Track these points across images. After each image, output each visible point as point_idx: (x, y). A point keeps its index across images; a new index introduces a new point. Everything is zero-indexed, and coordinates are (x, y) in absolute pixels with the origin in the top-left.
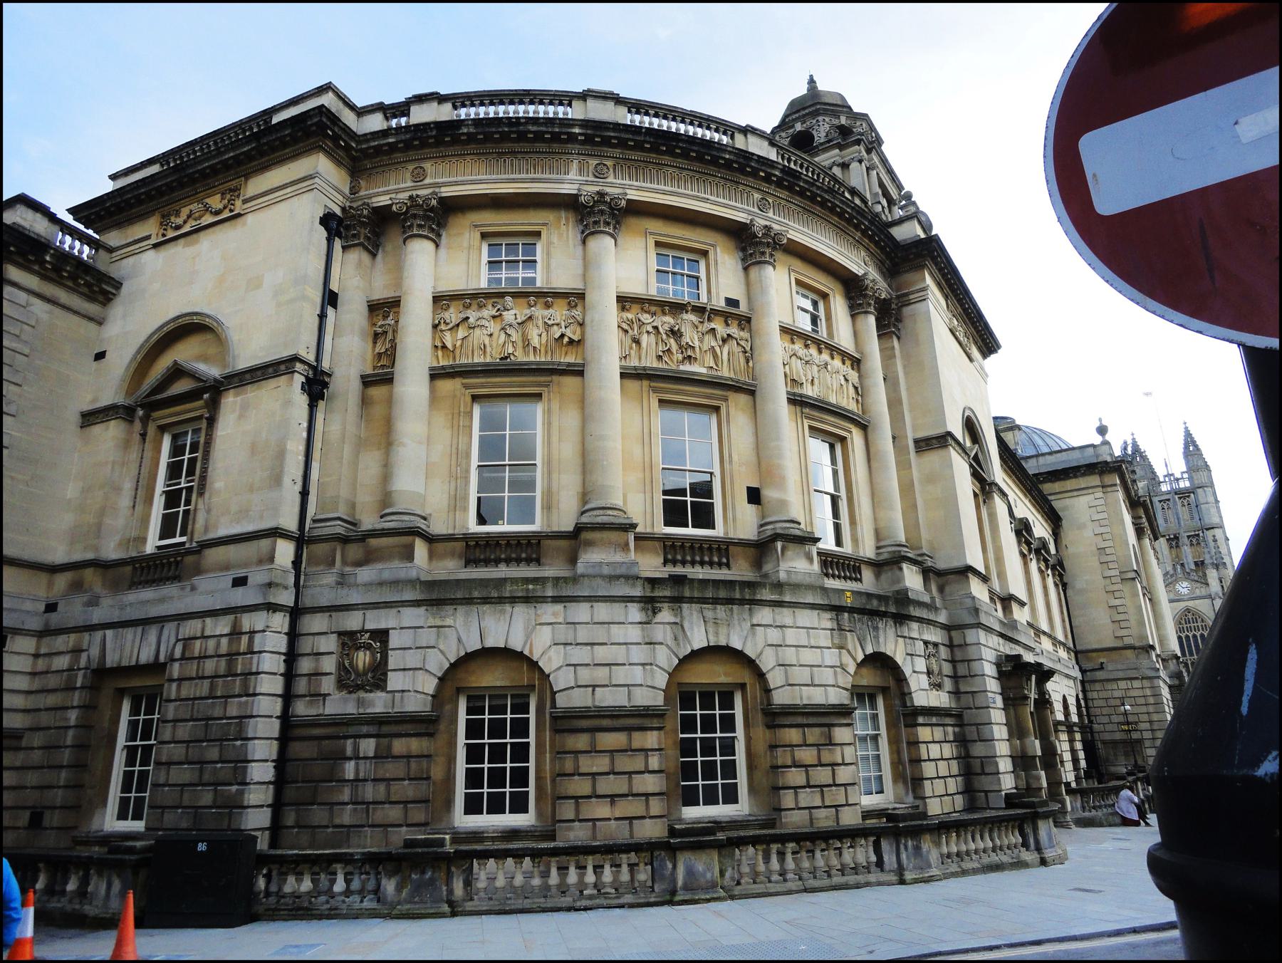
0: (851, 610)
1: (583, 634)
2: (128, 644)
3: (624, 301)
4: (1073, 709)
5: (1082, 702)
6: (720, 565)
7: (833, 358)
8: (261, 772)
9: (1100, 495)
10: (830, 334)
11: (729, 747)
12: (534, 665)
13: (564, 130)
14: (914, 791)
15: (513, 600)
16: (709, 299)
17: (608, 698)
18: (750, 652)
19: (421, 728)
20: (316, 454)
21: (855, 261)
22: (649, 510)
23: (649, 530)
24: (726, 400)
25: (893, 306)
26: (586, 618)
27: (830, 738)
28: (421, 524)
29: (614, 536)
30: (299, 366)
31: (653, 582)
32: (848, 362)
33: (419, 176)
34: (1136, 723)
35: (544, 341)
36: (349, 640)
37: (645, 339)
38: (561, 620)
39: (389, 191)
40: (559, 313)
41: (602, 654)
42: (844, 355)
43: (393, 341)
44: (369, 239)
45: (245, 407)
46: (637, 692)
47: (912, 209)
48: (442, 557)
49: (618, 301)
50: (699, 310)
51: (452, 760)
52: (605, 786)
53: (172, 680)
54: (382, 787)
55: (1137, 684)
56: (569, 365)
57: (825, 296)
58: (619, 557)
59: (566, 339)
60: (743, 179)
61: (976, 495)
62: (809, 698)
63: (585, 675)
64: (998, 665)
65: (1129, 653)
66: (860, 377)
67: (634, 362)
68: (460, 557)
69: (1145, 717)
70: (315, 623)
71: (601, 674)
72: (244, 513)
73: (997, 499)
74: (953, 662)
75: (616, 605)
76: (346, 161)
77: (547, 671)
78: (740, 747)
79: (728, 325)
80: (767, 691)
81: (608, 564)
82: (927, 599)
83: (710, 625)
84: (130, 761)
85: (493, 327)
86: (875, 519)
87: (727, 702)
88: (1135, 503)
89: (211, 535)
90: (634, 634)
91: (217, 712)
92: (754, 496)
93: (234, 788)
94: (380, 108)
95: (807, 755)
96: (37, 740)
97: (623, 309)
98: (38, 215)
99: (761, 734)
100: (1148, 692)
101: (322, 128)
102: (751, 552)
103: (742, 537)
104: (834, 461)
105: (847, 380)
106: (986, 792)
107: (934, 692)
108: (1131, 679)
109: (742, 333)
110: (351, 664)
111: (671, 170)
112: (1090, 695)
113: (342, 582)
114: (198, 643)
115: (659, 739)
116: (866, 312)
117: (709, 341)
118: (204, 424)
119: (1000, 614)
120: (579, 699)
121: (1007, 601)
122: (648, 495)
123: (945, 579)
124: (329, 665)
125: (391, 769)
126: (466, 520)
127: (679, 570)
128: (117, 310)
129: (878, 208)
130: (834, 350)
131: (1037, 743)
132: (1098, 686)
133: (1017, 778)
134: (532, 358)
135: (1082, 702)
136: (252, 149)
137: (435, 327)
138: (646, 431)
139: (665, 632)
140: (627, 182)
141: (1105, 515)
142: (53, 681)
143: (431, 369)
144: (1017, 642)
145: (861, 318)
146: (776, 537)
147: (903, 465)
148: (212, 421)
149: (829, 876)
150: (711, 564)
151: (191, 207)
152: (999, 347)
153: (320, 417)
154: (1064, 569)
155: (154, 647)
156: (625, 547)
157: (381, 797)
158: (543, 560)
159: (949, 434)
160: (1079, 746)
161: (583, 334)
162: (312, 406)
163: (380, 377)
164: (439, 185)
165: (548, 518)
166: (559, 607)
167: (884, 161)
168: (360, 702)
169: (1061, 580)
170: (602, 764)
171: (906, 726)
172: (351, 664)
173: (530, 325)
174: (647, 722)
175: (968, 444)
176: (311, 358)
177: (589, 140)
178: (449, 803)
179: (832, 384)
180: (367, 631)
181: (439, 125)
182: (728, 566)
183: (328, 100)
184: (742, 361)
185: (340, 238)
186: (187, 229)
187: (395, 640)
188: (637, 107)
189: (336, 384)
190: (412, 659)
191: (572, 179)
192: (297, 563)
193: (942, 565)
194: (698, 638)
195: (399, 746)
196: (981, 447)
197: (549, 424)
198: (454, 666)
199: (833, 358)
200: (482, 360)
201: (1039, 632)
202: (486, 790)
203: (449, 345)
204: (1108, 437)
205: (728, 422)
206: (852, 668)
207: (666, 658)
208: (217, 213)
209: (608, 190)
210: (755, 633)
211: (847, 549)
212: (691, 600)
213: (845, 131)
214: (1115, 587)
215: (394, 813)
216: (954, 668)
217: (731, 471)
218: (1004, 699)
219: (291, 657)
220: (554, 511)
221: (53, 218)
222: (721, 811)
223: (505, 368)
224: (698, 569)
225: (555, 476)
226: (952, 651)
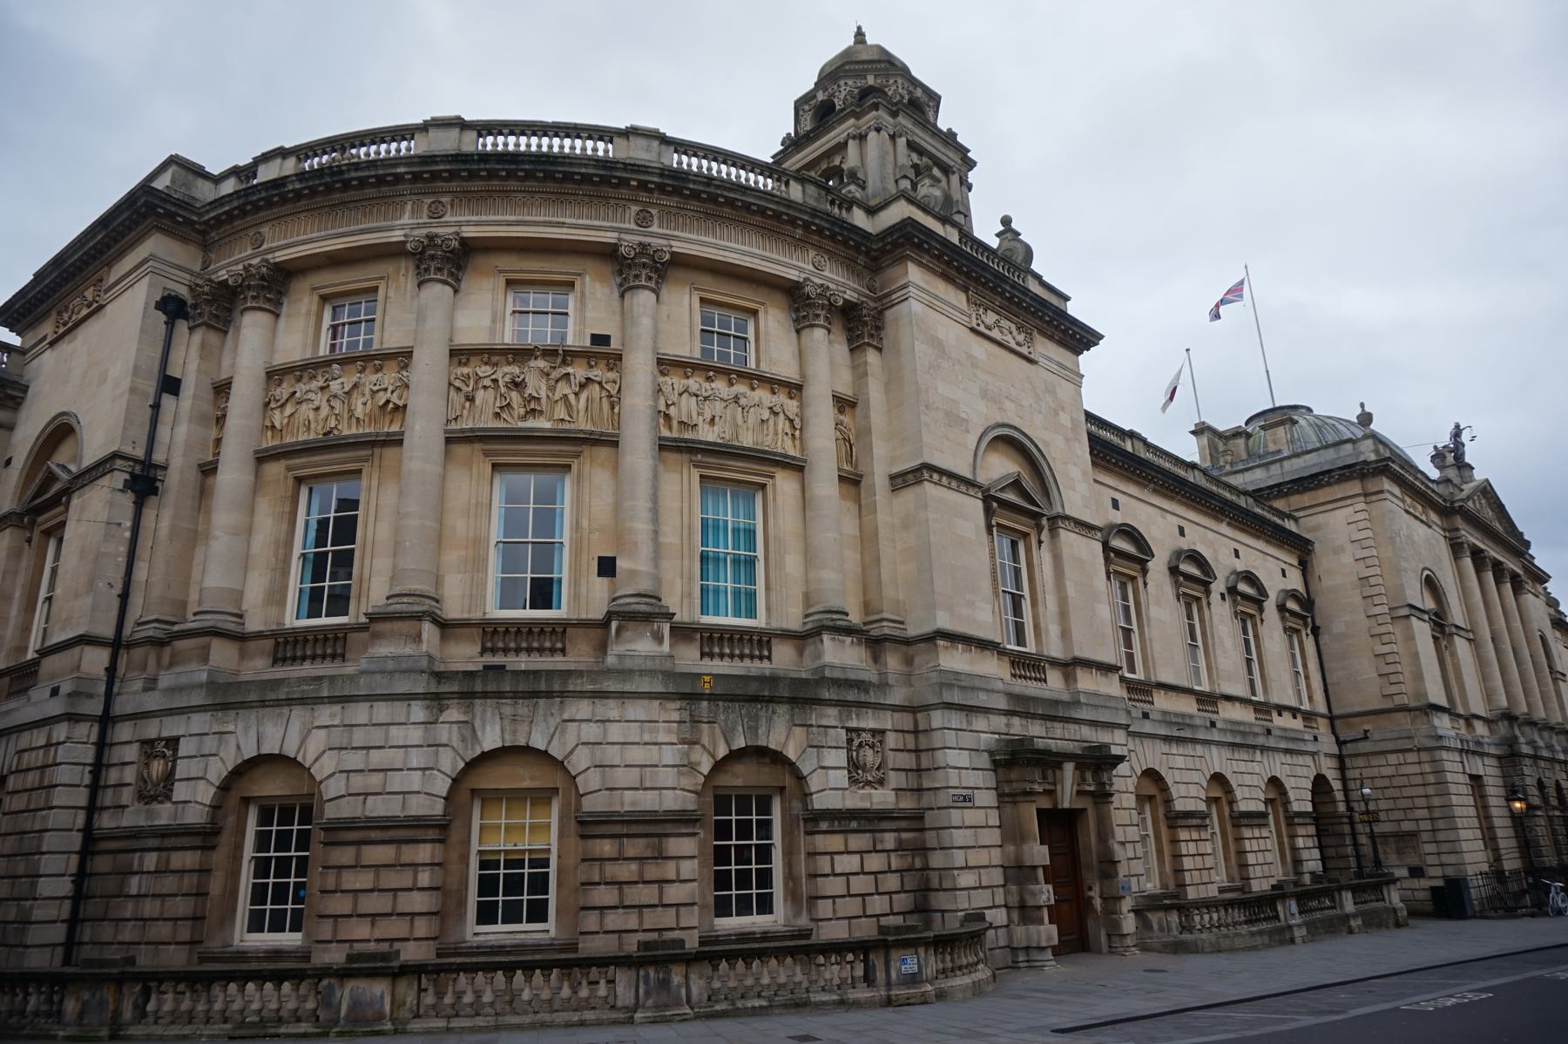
0: (712, 698)
1: (359, 737)
6: (553, 651)
9: (1362, 506)
11: (765, 854)
14: (809, 911)
15: (290, 702)
17: (378, 808)
26: (363, 719)
29: (405, 626)
30: (119, 463)
31: (470, 675)
36: (148, 747)
46: (413, 799)
51: (235, 874)
55: (1412, 757)
60: (611, 192)
62: (634, 803)
63: (358, 782)
65: (1401, 717)
66: (801, 406)
69: (1421, 802)
70: (124, 732)
71: (375, 781)
78: (777, 855)
83: (506, 721)
85: (319, 399)
86: (807, 581)
87: (765, 808)
90: (415, 735)
92: (607, 567)
95: (627, 871)
100: (1427, 768)
101: (151, 208)
106: (943, 911)
113: (151, 685)
117: (563, 389)
120: (348, 809)
123: (914, 647)
124: (130, 775)
127: (498, 659)
132: (1361, 762)
139: (450, 732)
141: (1369, 533)
143: (256, 452)
150: (541, 650)
162: (139, 506)
166: (337, 708)
170: (363, 880)
174: (419, 834)
176: (140, 453)
177: (417, 177)
178: (462, 916)
180: (162, 739)
182: (563, 651)
184: (606, 406)
187: (185, 748)
191: (404, 224)
194: (491, 739)
202: (500, 898)
203: (277, 425)
207: (450, 763)
212: (485, 695)
214: (1382, 629)
216: (918, 758)
222: (755, 922)
223: (330, 444)
224: (523, 657)
226: (917, 739)
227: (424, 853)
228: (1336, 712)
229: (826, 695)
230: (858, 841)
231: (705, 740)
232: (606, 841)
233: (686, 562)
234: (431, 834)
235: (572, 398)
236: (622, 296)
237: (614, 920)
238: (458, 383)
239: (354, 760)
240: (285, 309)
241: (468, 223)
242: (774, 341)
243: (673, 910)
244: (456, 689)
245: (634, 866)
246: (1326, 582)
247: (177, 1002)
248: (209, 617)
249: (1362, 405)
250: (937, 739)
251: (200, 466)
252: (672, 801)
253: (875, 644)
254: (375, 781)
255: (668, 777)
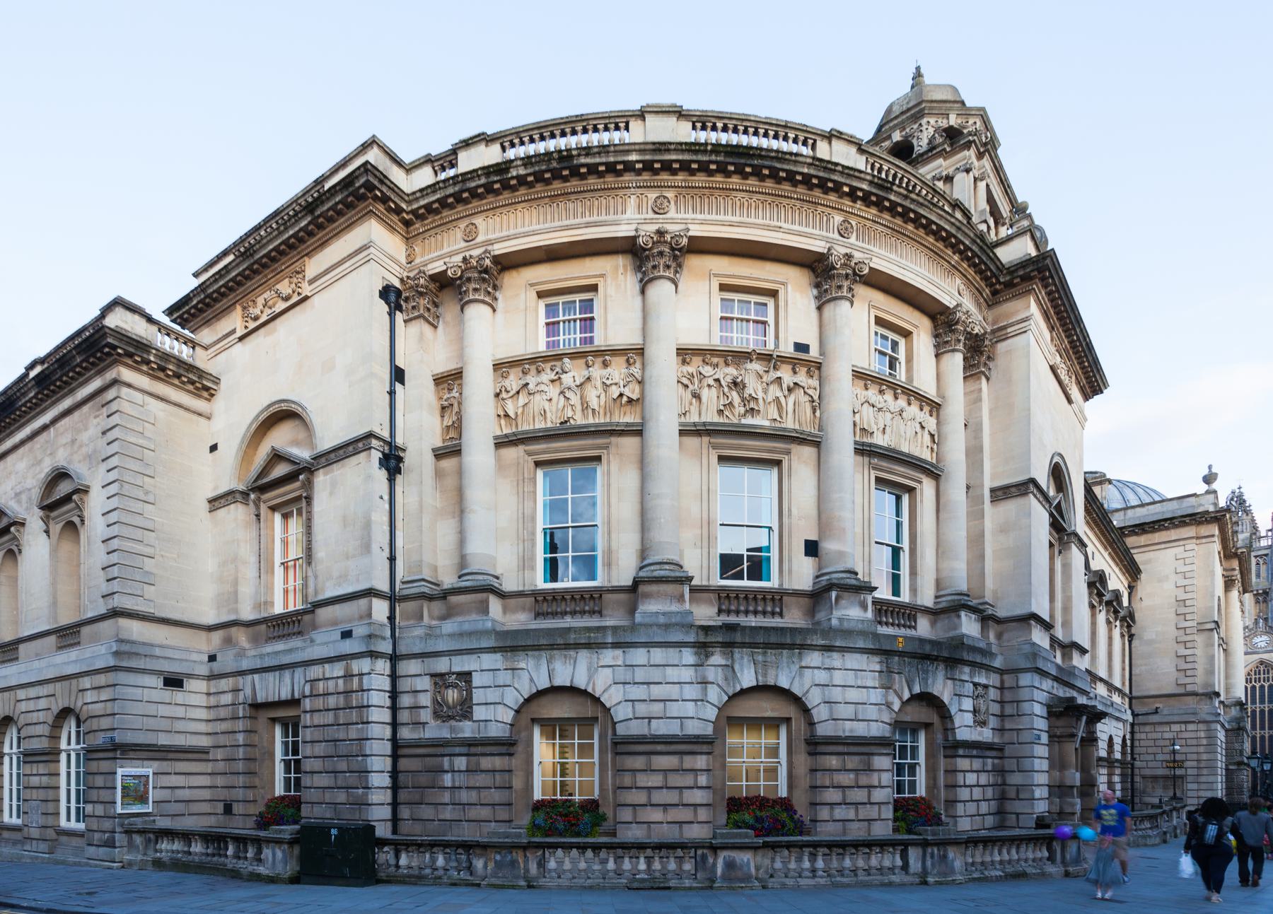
1: (640, 675)
2: (271, 686)
3: (685, 354)
4: (1117, 748)
5: (1129, 742)
6: (773, 614)
7: (909, 404)
8: (381, 780)
10: (910, 378)
11: (912, 768)
12: (596, 700)
13: (620, 159)
15: (577, 646)
16: (777, 346)
17: (660, 728)
18: (797, 690)
19: (503, 749)
20: (399, 524)
21: (948, 289)
22: (705, 565)
23: (705, 583)
24: (788, 453)
25: (987, 342)
27: (869, 764)
28: (495, 583)
30: (374, 443)
31: (706, 629)
32: (927, 409)
33: (469, 237)
34: (1183, 761)
35: (602, 403)
36: (440, 680)
37: (705, 393)
38: (620, 663)
39: (445, 251)
40: (617, 370)
41: (657, 691)
42: (922, 399)
43: (459, 413)
44: (429, 310)
45: (334, 484)
46: (689, 723)
47: (1025, 223)
48: (515, 611)
49: (678, 354)
50: (766, 358)
52: (658, 797)
53: (306, 712)
54: (474, 793)
55: (1191, 727)
56: (627, 424)
57: (906, 334)
58: (675, 607)
59: (625, 399)
61: (1051, 545)
62: (851, 731)
63: (642, 709)
64: (1049, 706)
65: (1190, 700)
66: (938, 424)
67: (694, 418)
68: (530, 610)
69: (1195, 757)
70: (409, 667)
71: (657, 709)
72: (343, 577)
73: (1074, 549)
74: (1002, 702)
75: (671, 650)
76: (400, 227)
77: (608, 705)
79: (795, 373)
80: (811, 724)
81: (664, 614)
82: (982, 645)
84: (288, 770)
85: (553, 391)
86: (937, 570)
88: (1228, 553)
89: (320, 597)
91: (342, 736)
92: (812, 548)
93: (360, 791)
94: (428, 160)
95: (847, 779)
96: (220, 754)
97: (684, 362)
98: (137, 317)
99: (802, 761)
100: (1202, 734)
102: (805, 601)
103: (801, 588)
104: (898, 513)
105: (923, 428)
106: (1018, 814)
107: (979, 728)
108: (1186, 723)
109: (810, 381)
110: (443, 699)
111: (740, 195)
112: (1137, 736)
114: (321, 683)
115: (708, 761)
116: (953, 351)
117: (774, 391)
118: (304, 504)
119: (1059, 660)
120: (636, 729)
121: (1071, 647)
122: (705, 550)
123: (1005, 626)
124: (425, 700)
125: (480, 780)
126: (534, 579)
127: (733, 619)
128: (219, 405)
129: (983, 227)
130: (912, 395)
131: (1078, 775)
133: (1051, 803)
134: (591, 421)
135: (1129, 742)
136: (309, 223)
137: (497, 395)
138: (705, 488)
139: (716, 673)
140: (690, 215)
142: (223, 713)
143: (496, 438)
144: (1073, 687)
145: (947, 358)
146: (830, 587)
147: (976, 514)
148: (309, 499)
149: (856, 875)
150: (764, 613)
151: (266, 295)
152: (1106, 385)
153: (399, 489)
154: (1134, 621)
155: (289, 688)
156: (681, 598)
157: (474, 800)
158: (604, 612)
159: (1033, 481)
160: (1116, 779)
161: (642, 392)
162: (391, 480)
163: (450, 451)
164: (490, 242)
165: (609, 574)
166: (619, 652)
167: (998, 169)
168: (452, 729)
169: (1129, 631)
170: (656, 780)
171: (945, 757)
172: (443, 699)
173: (588, 387)
175: (1052, 493)
177: (648, 167)
179: (904, 431)
181: (488, 170)
182: (781, 615)
183: (373, 156)
185: (401, 311)
186: (264, 318)
187: (477, 680)
188: (703, 121)
189: (409, 459)
190: (492, 695)
191: (629, 215)
192: (391, 618)
193: (1002, 613)
194: (748, 678)
195: (486, 763)
196: (1066, 496)
197: (609, 485)
198: (528, 701)
199: (909, 404)
200: (543, 426)
201: (1095, 678)
203: (512, 414)
204: (1215, 486)
205: (790, 476)
206: (896, 707)
207: (716, 695)
208: (287, 299)
209: (670, 228)
210: (808, 675)
211: (905, 597)
212: (743, 645)
213: (952, 134)
215: (485, 813)
216: (1002, 707)
217: (790, 524)
218: (1050, 737)
219: (394, 694)
220: (613, 567)
221: (150, 320)
223: (565, 432)
225: (614, 536)
227: (701, 762)
228: (1134, 694)
229: (966, 656)
230: (977, 764)
231: (896, 687)
232: (834, 757)
233: (867, 549)
234: (705, 748)
235: (783, 400)
236: (819, 308)
237: (839, 813)
238: (685, 381)
239: (637, 692)
240: (500, 305)
241: (694, 221)
242: (924, 364)
243: (876, 807)
244: (720, 640)
245: (852, 776)
246: (1146, 603)
247: (649, 864)
248: (480, 577)
249: (1210, 467)
250: (1024, 694)
251: (433, 450)
252: (876, 730)
253: (987, 619)
254: (657, 709)
255: (872, 712)
